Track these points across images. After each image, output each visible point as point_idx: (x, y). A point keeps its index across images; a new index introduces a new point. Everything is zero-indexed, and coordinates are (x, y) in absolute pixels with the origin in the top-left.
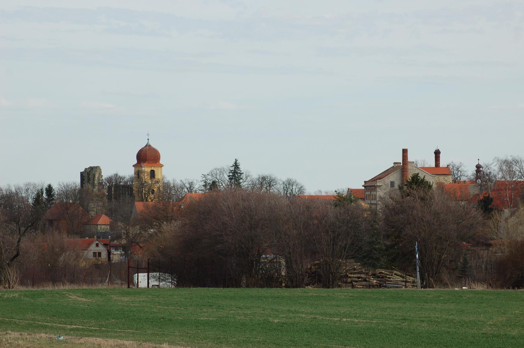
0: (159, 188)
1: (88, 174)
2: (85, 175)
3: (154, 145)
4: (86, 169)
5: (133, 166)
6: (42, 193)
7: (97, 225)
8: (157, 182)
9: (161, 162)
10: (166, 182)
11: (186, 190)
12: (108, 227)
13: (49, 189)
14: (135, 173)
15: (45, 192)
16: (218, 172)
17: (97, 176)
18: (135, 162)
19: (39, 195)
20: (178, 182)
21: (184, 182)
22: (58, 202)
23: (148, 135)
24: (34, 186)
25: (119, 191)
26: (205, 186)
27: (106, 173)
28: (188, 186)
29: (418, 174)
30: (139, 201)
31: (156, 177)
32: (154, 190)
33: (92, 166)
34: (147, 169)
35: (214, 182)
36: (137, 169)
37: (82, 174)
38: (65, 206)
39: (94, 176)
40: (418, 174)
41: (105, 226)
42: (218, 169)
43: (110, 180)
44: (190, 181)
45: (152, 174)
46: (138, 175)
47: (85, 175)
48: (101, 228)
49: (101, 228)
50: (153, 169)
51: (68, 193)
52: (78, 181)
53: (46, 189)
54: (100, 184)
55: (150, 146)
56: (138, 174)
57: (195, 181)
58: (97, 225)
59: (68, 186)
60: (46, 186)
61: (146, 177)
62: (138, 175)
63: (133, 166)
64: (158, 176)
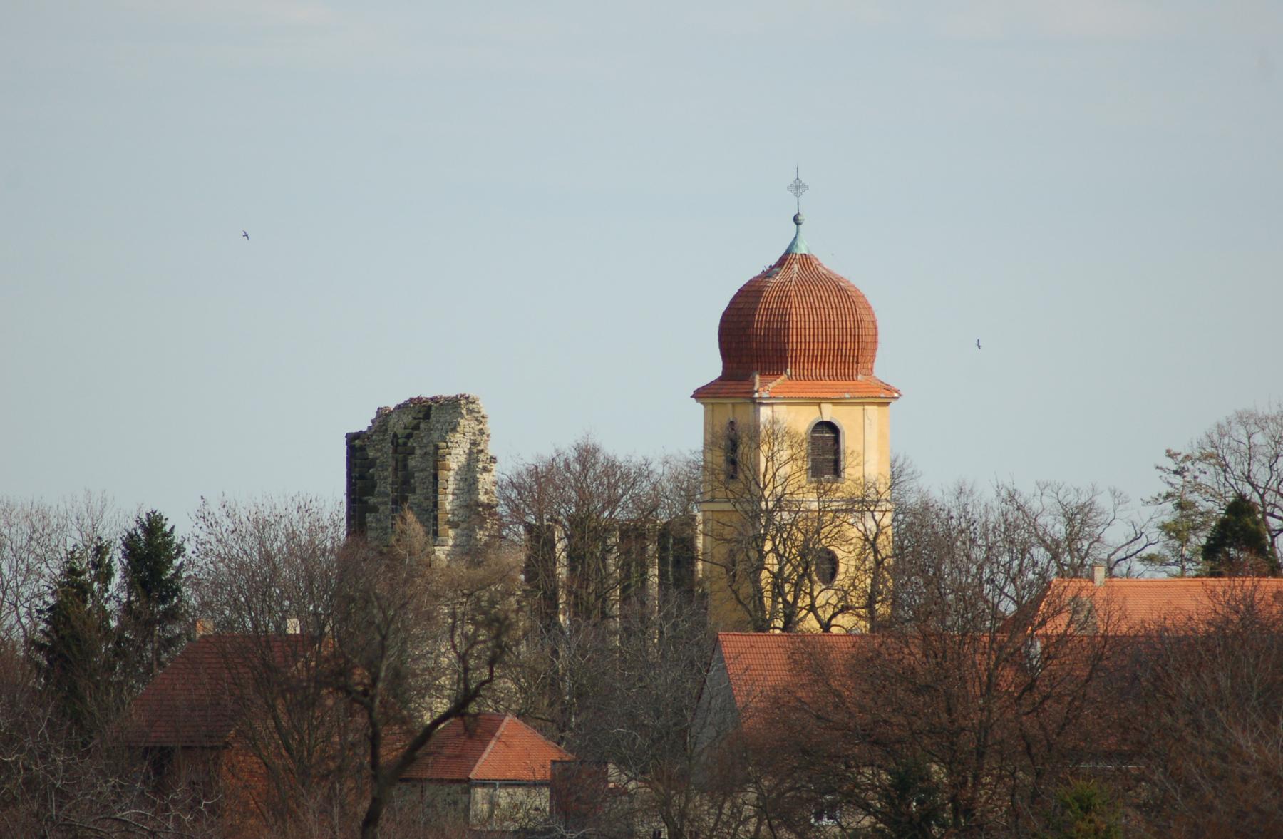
0: (870, 543)
1: (402, 447)
2: (382, 453)
3: (833, 261)
4: (383, 417)
5: (699, 395)
6: (106, 576)
7: (468, 784)
8: (860, 504)
9: (885, 367)
10: (912, 500)
11: (1039, 554)
12: (542, 799)
13: (150, 550)
14: (710, 445)
15: (117, 558)
16: (1259, 439)
17: (456, 459)
18: (712, 367)
19: (75, 587)
20: (986, 503)
21: (1035, 505)
22: (205, 627)
23: (798, 188)
24: (40, 529)
25: (627, 562)
26: (1174, 531)
27: (516, 440)
28: (1058, 530)
29: (1164, 527)
30: (739, 627)
31: (851, 471)
32: (834, 561)
33: (427, 393)
34: (786, 415)
35: (1240, 507)
36: (726, 414)
37: (357, 446)
38: (252, 662)
39: (436, 461)
40: (1164, 527)
41: (520, 793)
42: (1262, 423)
43: (540, 484)
44: (1072, 500)
45: (826, 448)
46: (733, 445)
47: (382, 453)
48: (493, 804)
49: (493, 804)
50: (829, 413)
51: (261, 575)
52: (329, 491)
53: (130, 543)
54: (474, 511)
55: (806, 261)
56: (732, 450)
57: (1104, 501)
58: (468, 784)
59: (262, 526)
60: (118, 524)
61: (782, 470)
62: (733, 445)
63: (699, 395)
64: (867, 459)
